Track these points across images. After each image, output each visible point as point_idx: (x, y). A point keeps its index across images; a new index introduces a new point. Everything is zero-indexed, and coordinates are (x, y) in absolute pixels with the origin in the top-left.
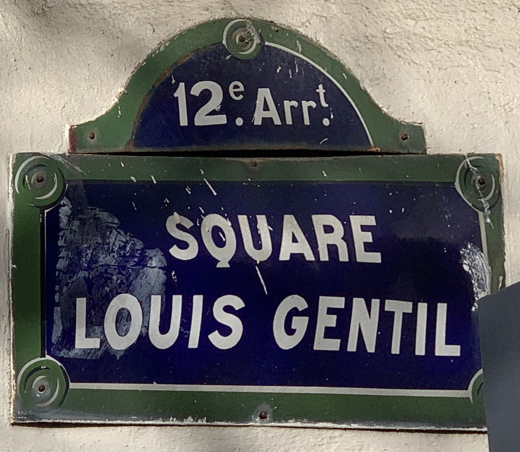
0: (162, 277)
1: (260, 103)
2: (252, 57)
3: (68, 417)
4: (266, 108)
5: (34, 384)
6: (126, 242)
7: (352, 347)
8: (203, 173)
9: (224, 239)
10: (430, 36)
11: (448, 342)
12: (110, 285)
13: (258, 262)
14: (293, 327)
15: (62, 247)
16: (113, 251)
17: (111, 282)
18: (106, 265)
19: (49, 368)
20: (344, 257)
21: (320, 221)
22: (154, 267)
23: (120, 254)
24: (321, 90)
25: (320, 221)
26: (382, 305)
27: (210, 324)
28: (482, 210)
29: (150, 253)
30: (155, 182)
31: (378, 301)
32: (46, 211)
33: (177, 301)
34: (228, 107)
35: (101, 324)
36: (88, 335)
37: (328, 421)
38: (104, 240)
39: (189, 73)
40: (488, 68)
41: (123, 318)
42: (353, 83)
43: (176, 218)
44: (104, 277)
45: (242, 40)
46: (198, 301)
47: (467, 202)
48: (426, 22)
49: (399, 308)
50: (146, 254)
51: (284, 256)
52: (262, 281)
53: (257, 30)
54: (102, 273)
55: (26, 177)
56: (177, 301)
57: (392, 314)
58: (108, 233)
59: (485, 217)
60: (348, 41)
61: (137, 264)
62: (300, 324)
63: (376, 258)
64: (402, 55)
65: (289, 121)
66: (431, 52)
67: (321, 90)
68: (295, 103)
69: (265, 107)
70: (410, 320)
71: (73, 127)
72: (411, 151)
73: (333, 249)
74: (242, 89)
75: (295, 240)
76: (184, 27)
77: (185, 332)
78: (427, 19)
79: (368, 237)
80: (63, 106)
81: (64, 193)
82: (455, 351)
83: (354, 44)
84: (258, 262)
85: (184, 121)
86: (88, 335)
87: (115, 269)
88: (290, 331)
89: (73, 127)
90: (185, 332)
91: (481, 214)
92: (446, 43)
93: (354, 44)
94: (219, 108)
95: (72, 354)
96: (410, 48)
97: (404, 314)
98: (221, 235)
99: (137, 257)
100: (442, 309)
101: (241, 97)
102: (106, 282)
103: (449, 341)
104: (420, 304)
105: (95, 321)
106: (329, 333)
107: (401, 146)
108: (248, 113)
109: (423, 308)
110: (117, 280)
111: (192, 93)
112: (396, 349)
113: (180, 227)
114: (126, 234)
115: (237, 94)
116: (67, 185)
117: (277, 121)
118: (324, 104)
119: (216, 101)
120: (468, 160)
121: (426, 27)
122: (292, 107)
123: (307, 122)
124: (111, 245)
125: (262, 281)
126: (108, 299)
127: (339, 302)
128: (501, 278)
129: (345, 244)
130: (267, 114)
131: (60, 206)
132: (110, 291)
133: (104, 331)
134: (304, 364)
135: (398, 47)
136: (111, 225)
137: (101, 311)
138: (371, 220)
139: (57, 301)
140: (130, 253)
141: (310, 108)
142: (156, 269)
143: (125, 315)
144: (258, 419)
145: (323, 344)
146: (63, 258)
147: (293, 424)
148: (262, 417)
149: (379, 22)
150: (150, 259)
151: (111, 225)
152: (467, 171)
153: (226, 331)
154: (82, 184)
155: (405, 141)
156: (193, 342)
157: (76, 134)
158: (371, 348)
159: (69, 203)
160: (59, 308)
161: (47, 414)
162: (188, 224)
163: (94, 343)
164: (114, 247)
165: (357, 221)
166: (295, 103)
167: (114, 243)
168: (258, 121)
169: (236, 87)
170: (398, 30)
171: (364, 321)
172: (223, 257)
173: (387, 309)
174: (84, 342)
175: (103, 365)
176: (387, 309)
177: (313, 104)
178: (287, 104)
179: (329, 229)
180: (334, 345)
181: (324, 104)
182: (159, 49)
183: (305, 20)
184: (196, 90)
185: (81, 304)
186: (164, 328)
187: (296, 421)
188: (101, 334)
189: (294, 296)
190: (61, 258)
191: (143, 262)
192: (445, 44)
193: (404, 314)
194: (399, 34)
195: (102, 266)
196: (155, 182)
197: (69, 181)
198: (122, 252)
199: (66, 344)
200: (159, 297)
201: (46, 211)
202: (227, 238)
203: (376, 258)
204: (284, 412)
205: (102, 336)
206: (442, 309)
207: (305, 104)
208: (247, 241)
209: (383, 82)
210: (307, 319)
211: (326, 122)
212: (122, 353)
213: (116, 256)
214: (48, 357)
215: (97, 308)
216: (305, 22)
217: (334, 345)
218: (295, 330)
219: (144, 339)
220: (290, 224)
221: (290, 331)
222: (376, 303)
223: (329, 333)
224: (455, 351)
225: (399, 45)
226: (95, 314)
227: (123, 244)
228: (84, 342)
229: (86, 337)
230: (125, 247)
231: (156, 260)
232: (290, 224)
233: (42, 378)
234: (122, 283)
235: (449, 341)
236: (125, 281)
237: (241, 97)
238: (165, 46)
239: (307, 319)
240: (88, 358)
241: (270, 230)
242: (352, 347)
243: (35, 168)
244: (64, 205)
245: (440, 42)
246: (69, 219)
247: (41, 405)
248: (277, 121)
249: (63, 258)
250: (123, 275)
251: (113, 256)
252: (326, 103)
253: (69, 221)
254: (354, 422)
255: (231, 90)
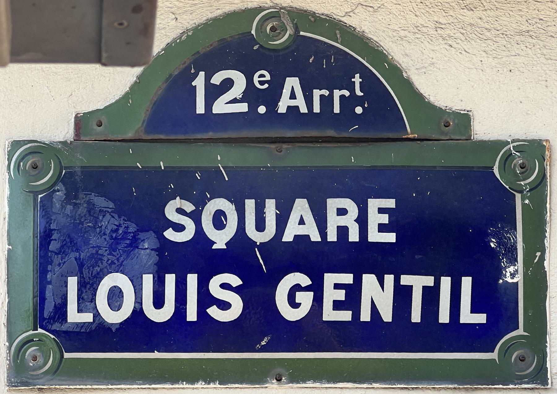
0: (155, 258)
1: (286, 92)
2: (279, 48)
3: (64, 383)
4: (293, 96)
5: (27, 354)
6: (119, 226)
7: (365, 316)
8: (219, 158)
9: (225, 223)
10: (488, 27)
11: (473, 311)
12: (100, 265)
13: (258, 244)
14: (297, 301)
15: (55, 230)
16: (105, 234)
17: (102, 262)
18: (97, 246)
19: (41, 340)
20: (354, 236)
21: (333, 204)
22: (146, 249)
23: (112, 237)
24: (357, 79)
25: (333, 204)
26: (397, 281)
27: (206, 299)
28: (521, 192)
29: (141, 235)
30: (163, 168)
31: (392, 277)
32: (40, 196)
33: (170, 280)
34: (251, 95)
35: (93, 300)
36: (80, 311)
37: (348, 382)
38: (96, 223)
39: (210, 62)
40: (547, 57)
41: (115, 296)
42: (395, 72)
43: (177, 203)
44: (97, 258)
45: (273, 29)
46: (192, 280)
47: (505, 185)
48: (484, 13)
49: (417, 283)
50: (139, 236)
51: (288, 237)
52: (261, 261)
53: (292, 20)
54: (92, 254)
55: (22, 164)
56: (170, 280)
57: (409, 288)
58: (101, 218)
59: (523, 199)
60: (396, 30)
61: (130, 245)
62: (306, 299)
63: (391, 238)
64: (454, 45)
65: (317, 109)
66: (486, 41)
67: (357, 79)
68: (326, 92)
69: (292, 95)
70: (431, 295)
71: (79, 115)
72: (453, 137)
73: (343, 231)
74: (268, 77)
75: (302, 222)
76: (211, 16)
77: (181, 307)
78: (486, 10)
79: (385, 219)
80: (70, 93)
81: (59, 179)
82: (481, 318)
83: (402, 33)
84: (258, 244)
85: (200, 109)
86: (80, 311)
87: (106, 250)
88: (294, 304)
89: (79, 115)
90: (181, 307)
91: (518, 196)
92: (505, 33)
93: (402, 33)
94: (241, 96)
95: (64, 328)
96: (463, 39)
97: (424, 288)
98: (223, 219)
99: (129, 239)
100: (467, 283)
101: (266, 86)
102: (96, 262)
103: (475, 310)
104: (443, 278)
105: (87, 298)
106: (338, 305)
107: (443, 133)
108: (272, 103)
109: (446, 282)
110: (108, 261)
111: (213, 81)
112: (416, 316)
113: (180, 211)
114: (120, 217)
115: (262, 83)
116: (64, 171)
117: (304, 109)
118: (359, 93)
119: (238, 90)
120: (511, 145)
121: (484, 17)
122: (322, 96)
123: (337, 110)
124: (103, 228)
125: (261, 261)
126: (99, 278)
127: (348, 278)
128: (538, 254)
129: (356, 226)
130: (293, 103)
131: (55, 191)
132: (101, 270)
133: (96, 307)
134: (311, 333)
135: (450, 37)
136: (105, 209)
137: (92, 289)
138: (391, 203)
139: (49, 280)
140: (123, 236)
141: (342, 97)
142: (148, 251)
143: (117, 292)
144: (275, 381)
145: (330, 314)
146: (55, 240)
147: (311, 385)
148: (279, 380)
149: (432, 13)
150: (142, 241)
151: (105, 209)
152: (508, 156)
153: (224, 306)
154: (79, 169)
155: (447, 128)
156: (192, 315)
157: (81, 122)
158: (387, 316)
159: (63, 189)
160: (50, 286)
161: (41, 381)
162: (189, 207)
163: (88, 317)
164: (106, 230)
165: (374, 204)
166: (326, 92)
167: (107, 226)
168: (282, 108)
169: (262, 76)
170: (452, 20)
171: (378, 294)
172: (220, 239)
173: (403, 282)
174: (75, 316)
175: (98, 336)
176: (403, 282)
177: (347, 93)
178: (317, 94)
179: (342, 212)
180: (346, 316)
181: (359, 93)
182: (181, 38)
183: (349, 10)
184: (217, 79)
185: (73, 282)
186: (159, 302)
187: (315, 381)
188: (94, 310)
189: (296, 273)
190: (52, 240)
191: (134, 243)
192: (503, 34)
193: (424, 288)
194: (453, 25)
195: (93, 247)
196: (163, 168)
197: (66, 168)
198: (114, 235)
199: (59, 318)
200: (151, 276)
201: (40, 196)
202: (221, 223)
203: (391, 238)
204: (299, 374)
205: (95, 311)
206: (467, 283)
207: (337, 93)
208: (249, 224)
209: (431, 70)
210: (311, 294)
211: (359, 110)
212: (118, 326)
213: (108, 239)
214: (40, 330)
215: (88, 286)
216: (349, 12)
217: (346, 316)
218: (300, 304)
219: (138, 312)
220: (301, 207)
221: (294, 304)
222: (389, 279)
223: (338, 305)
224: (481, 318)
225: (452, 35)
226: (86, 292)
227: (116, 227)
228: (75, 316)
229: (78, 312)
230: (116, 231)
231: (148, 243)
232: (301, 207)
233: (35, 350)
234: (113, 263)
235: (475, 310)
236: (116, 261)
237: (266, 86)
238: (188, 36)
239: (311, 294)
240: (82, 331)
241: (276, 213)
242: (365, 316)
243: (31, 156)
244: (58, 191)
245: (498, 32)
246: (62, 205)
247: (35, 373)
248: (304, 109)
249: (55, 240)
250: (114, 255)
251: (105, 239)
252: (361, 91)
253: (63, 207)
254: (376, 382)
255: (256, 79)
